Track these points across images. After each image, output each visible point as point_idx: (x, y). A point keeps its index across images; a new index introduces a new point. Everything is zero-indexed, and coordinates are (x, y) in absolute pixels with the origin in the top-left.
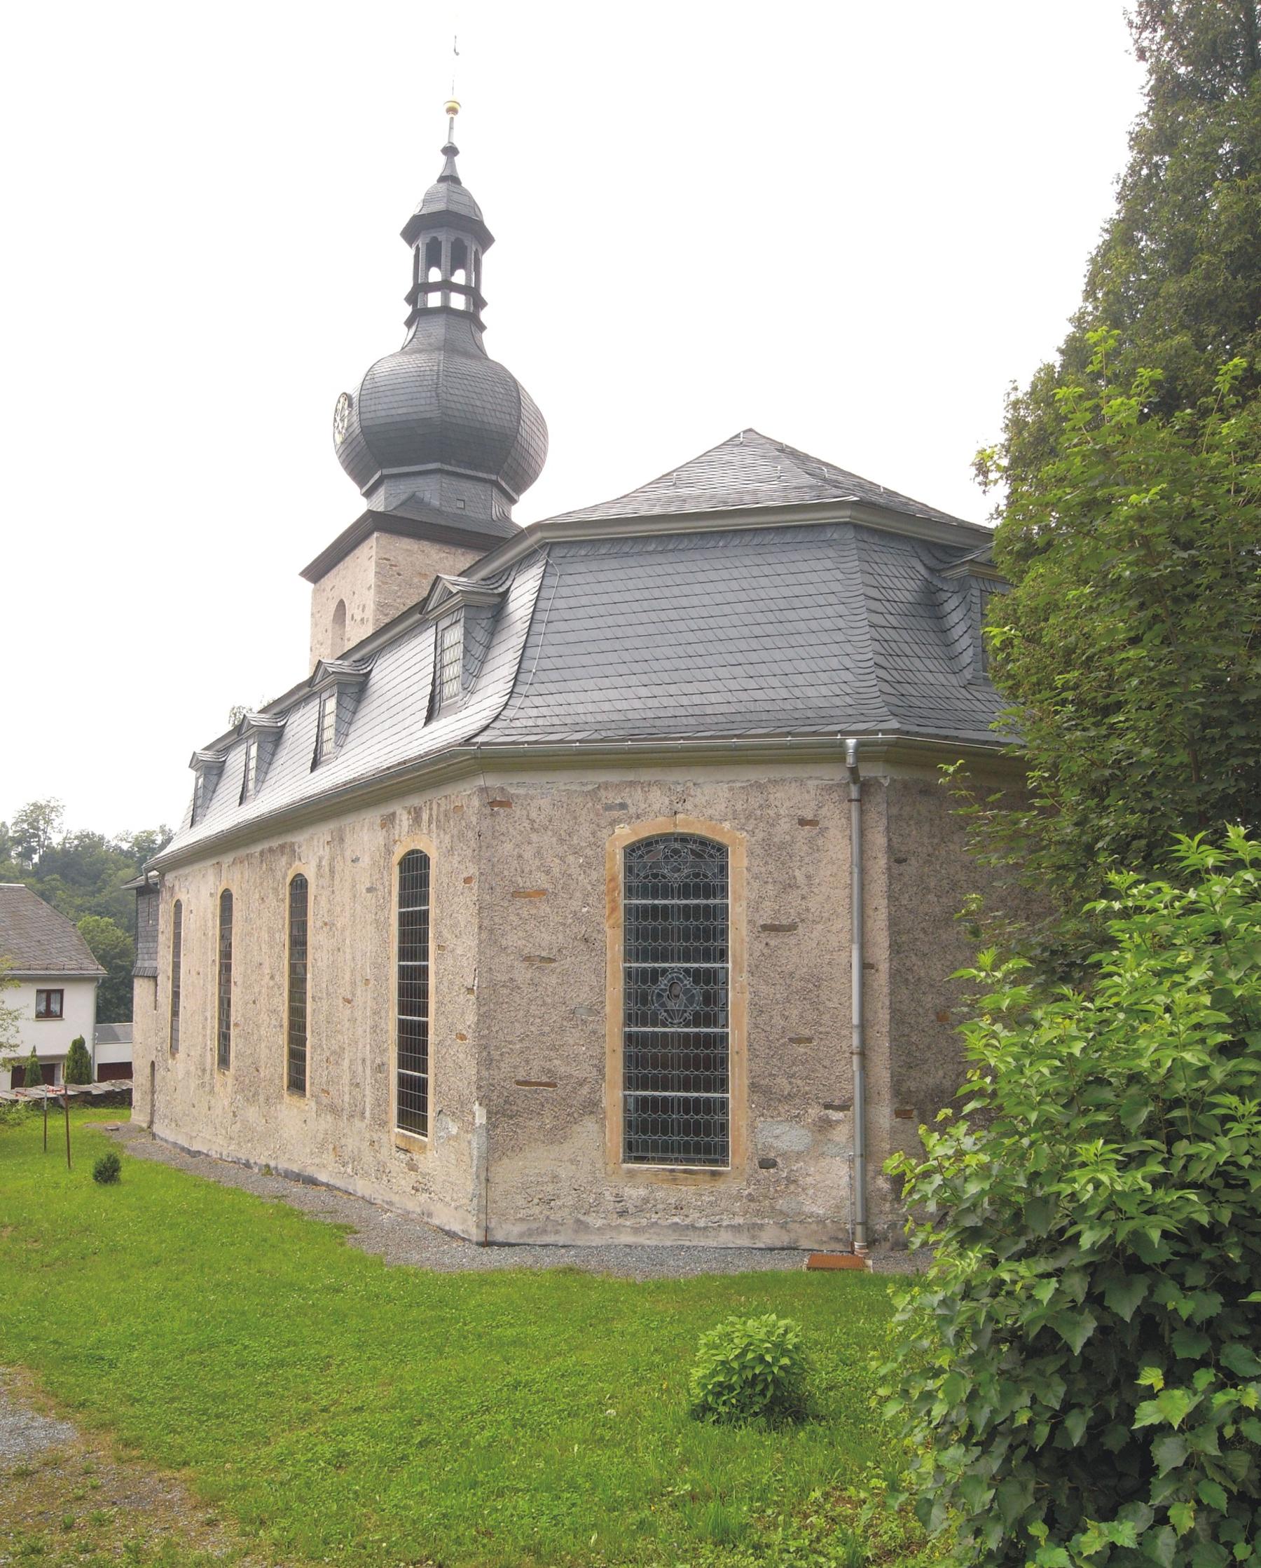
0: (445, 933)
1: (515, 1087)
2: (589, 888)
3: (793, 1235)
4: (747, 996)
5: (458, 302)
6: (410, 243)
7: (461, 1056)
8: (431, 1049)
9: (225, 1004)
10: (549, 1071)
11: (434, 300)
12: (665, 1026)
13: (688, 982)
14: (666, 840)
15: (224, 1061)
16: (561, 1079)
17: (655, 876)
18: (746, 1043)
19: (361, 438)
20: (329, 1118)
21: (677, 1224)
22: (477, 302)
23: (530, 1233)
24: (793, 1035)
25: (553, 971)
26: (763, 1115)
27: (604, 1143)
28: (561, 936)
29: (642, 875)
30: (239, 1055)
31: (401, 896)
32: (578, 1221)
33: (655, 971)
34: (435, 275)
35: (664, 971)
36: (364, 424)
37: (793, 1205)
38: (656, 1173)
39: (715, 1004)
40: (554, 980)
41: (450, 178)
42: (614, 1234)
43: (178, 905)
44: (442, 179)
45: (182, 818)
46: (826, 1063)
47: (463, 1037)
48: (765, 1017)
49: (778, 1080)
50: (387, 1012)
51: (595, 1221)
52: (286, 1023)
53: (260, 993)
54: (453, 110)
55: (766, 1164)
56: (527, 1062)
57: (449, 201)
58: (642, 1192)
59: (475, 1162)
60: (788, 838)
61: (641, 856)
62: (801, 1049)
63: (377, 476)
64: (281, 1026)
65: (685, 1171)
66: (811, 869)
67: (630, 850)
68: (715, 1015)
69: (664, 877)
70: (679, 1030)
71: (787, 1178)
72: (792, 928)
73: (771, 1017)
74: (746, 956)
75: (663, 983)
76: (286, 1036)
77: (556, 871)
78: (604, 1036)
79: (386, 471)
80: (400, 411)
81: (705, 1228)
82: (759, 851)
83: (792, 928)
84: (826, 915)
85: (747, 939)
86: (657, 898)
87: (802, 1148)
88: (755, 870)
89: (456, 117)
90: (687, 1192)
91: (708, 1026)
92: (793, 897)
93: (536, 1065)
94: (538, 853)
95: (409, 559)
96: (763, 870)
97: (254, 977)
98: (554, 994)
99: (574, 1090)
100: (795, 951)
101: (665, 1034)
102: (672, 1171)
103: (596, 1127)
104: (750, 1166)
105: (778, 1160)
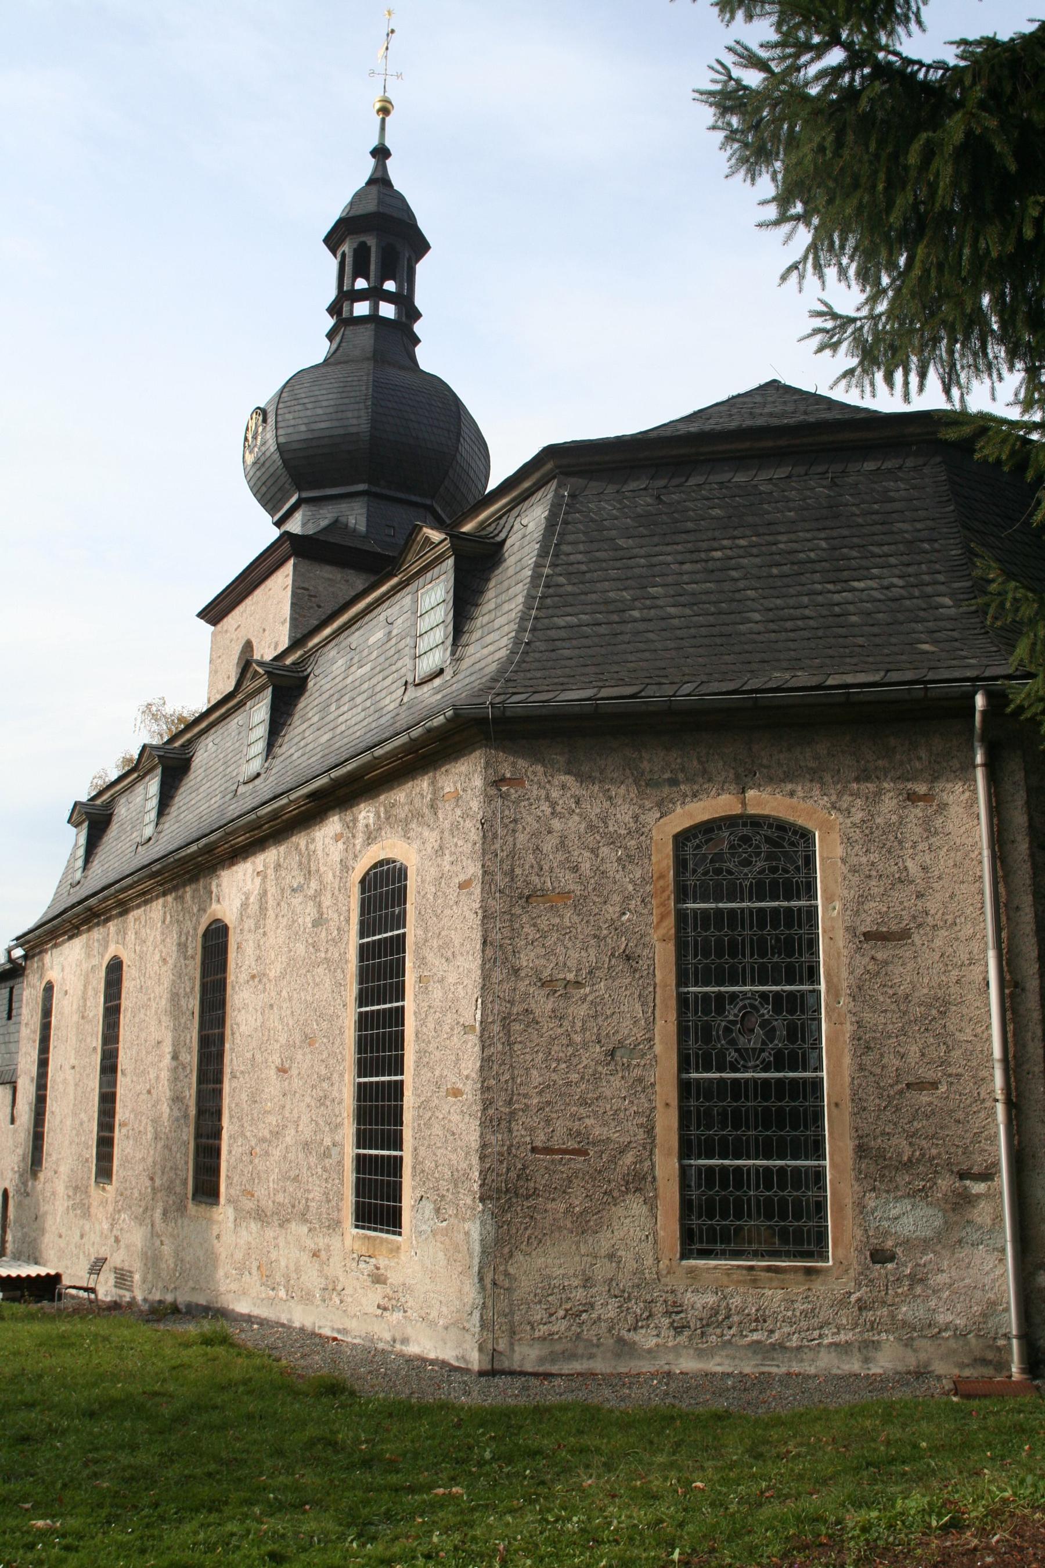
0: (430, 957)
1: (531, 1156)
2: (630, 887)
3: (923, 1356)
4: (849, 1028)
5: (387, 310)
6: (334, 251)
7: (455, 1118)
8: (408, 1116)
9: (108, 1100)
10: (579, 1133)
11: (361, 309)
12: (735, 1070)
13: (766, 1011)
14: (732, 825)
15: (104, 1170)
16: (594, 1144)
17: (718, 872)
18: (848, 1091)
19: (277, 456)
20: (254, 1226)
21: (758, 1342)
22: (410, 313)
23: (553, 1357)
24: (911, 1079)
25: (584, 999)
26: (874, 1189)
27: (655, 1233)
28: (592, 952)
29: (700, 870)
30: (126, 1161)
31: (362, 923)
32: (621, 1341)
33: (720, 996)
34: (361, 284)
35: (733, 996)
36: (282, 440)
37: (921, 1313)
38: (728, 1272)
39: (803, 1040)
40: (582, 1010)
41: (380, 181)
42: (671, 1357)
43: (49, 988)
44: (371, 182)
45: (273, 394)
46: (960, 1115)
47: (456, 1093)
48: (872, 1056)
49: (894, 1141)
50: (341, 1075)
51: (646, 1339)
52: (193, 1111)
53: (158, 1078)
54: (385, 110)
55: (880, 1256)
56: (548, 1121)
57: (380, 202)
58: (711, 1299)
59: (476, 1261)
60: (894, 818)
61: (698, 847)
62: (924, 1098)
63: (293, 500)
64: (186, 1116)
65: (769, 1269)
66: (927, 858)
67: (681, 839)
68: (804, 1055)
69: (730, 872)
70: (756, 1075)
71: (912, 1277)
72: (904, 935)
73: (882, 1055)
74: (844, 974)
75: (733, 1012)
76: (192, 1129)
77: (585, 867)
78: (653, 1085)
79: (305, 495)
80: (323, 425)
81: (799, 1348)
82: (856, 835)
83: (904, 935)
84: (950, 918)
85: (845, 952)
86: (721, 901)
87: (929, 1233)
88: (854, 860)
89: (388, 119)
90: (773, 1297)
91: (795, 1070)
92: (903, 895)
93: (560, 1126)
94: (562, 845)
95: (331, 589)
96: (864, 860)
97: (150, 1058)
98: (584, 1030)
99: (613, 1160)
100: (910, 966)
101: (735, 1081)
102: (751, 1268)
103: (645, 1209)
104: (855, 1261)
105: (899, 1251)
